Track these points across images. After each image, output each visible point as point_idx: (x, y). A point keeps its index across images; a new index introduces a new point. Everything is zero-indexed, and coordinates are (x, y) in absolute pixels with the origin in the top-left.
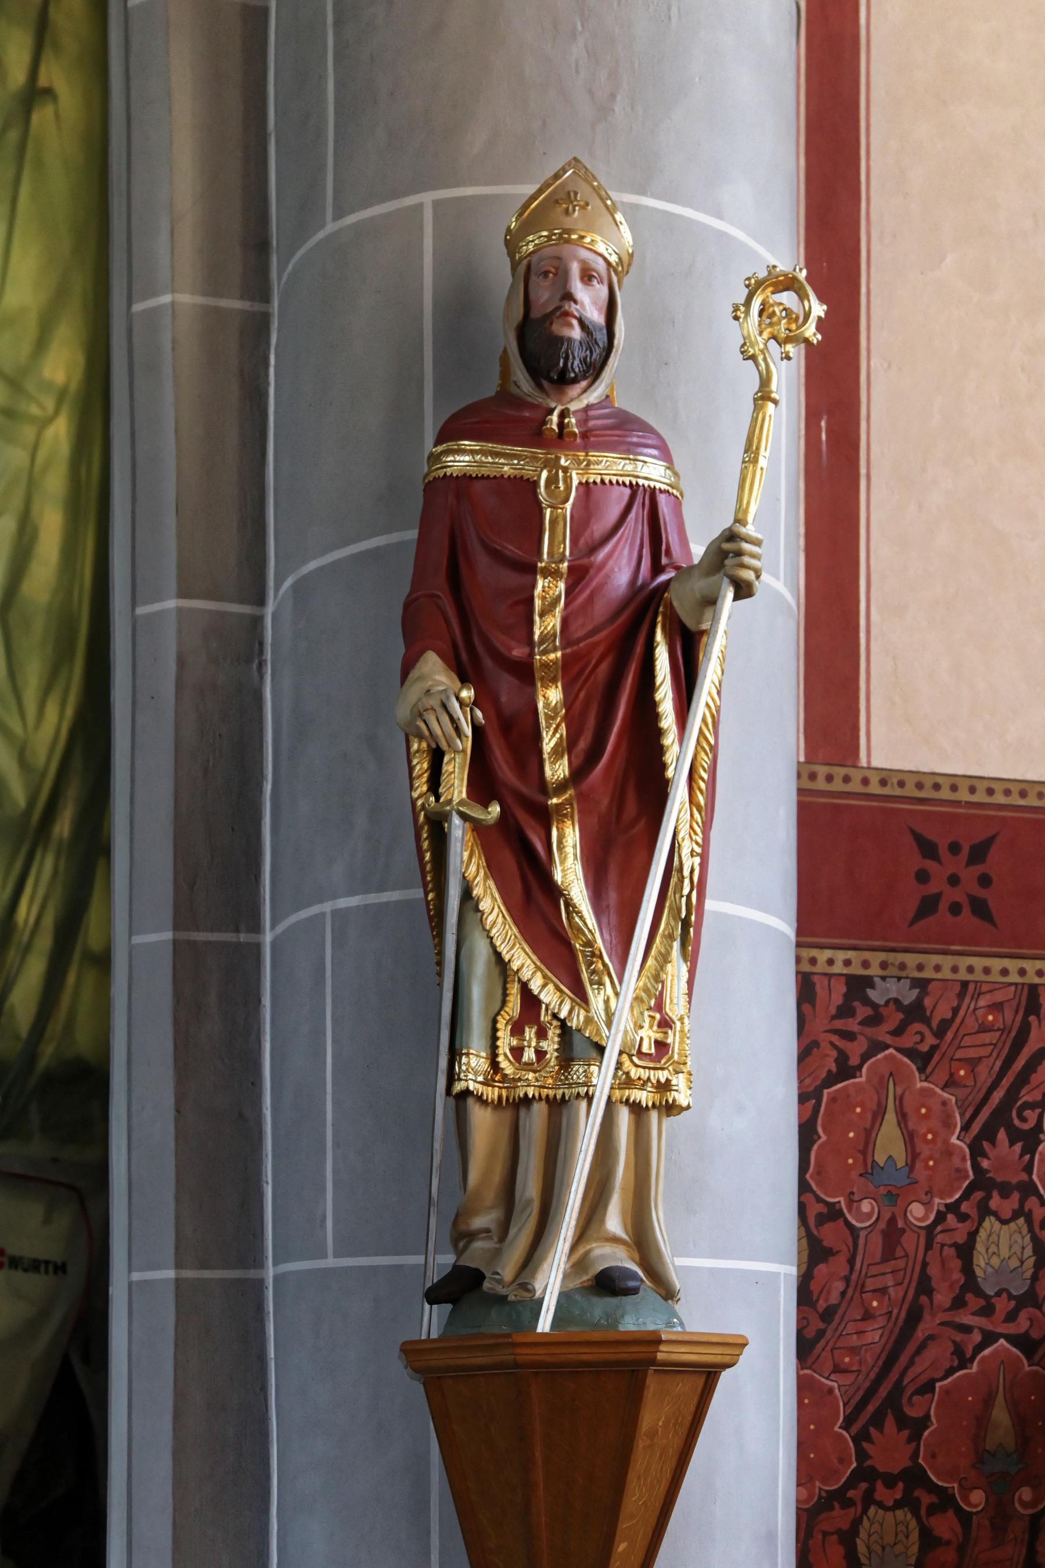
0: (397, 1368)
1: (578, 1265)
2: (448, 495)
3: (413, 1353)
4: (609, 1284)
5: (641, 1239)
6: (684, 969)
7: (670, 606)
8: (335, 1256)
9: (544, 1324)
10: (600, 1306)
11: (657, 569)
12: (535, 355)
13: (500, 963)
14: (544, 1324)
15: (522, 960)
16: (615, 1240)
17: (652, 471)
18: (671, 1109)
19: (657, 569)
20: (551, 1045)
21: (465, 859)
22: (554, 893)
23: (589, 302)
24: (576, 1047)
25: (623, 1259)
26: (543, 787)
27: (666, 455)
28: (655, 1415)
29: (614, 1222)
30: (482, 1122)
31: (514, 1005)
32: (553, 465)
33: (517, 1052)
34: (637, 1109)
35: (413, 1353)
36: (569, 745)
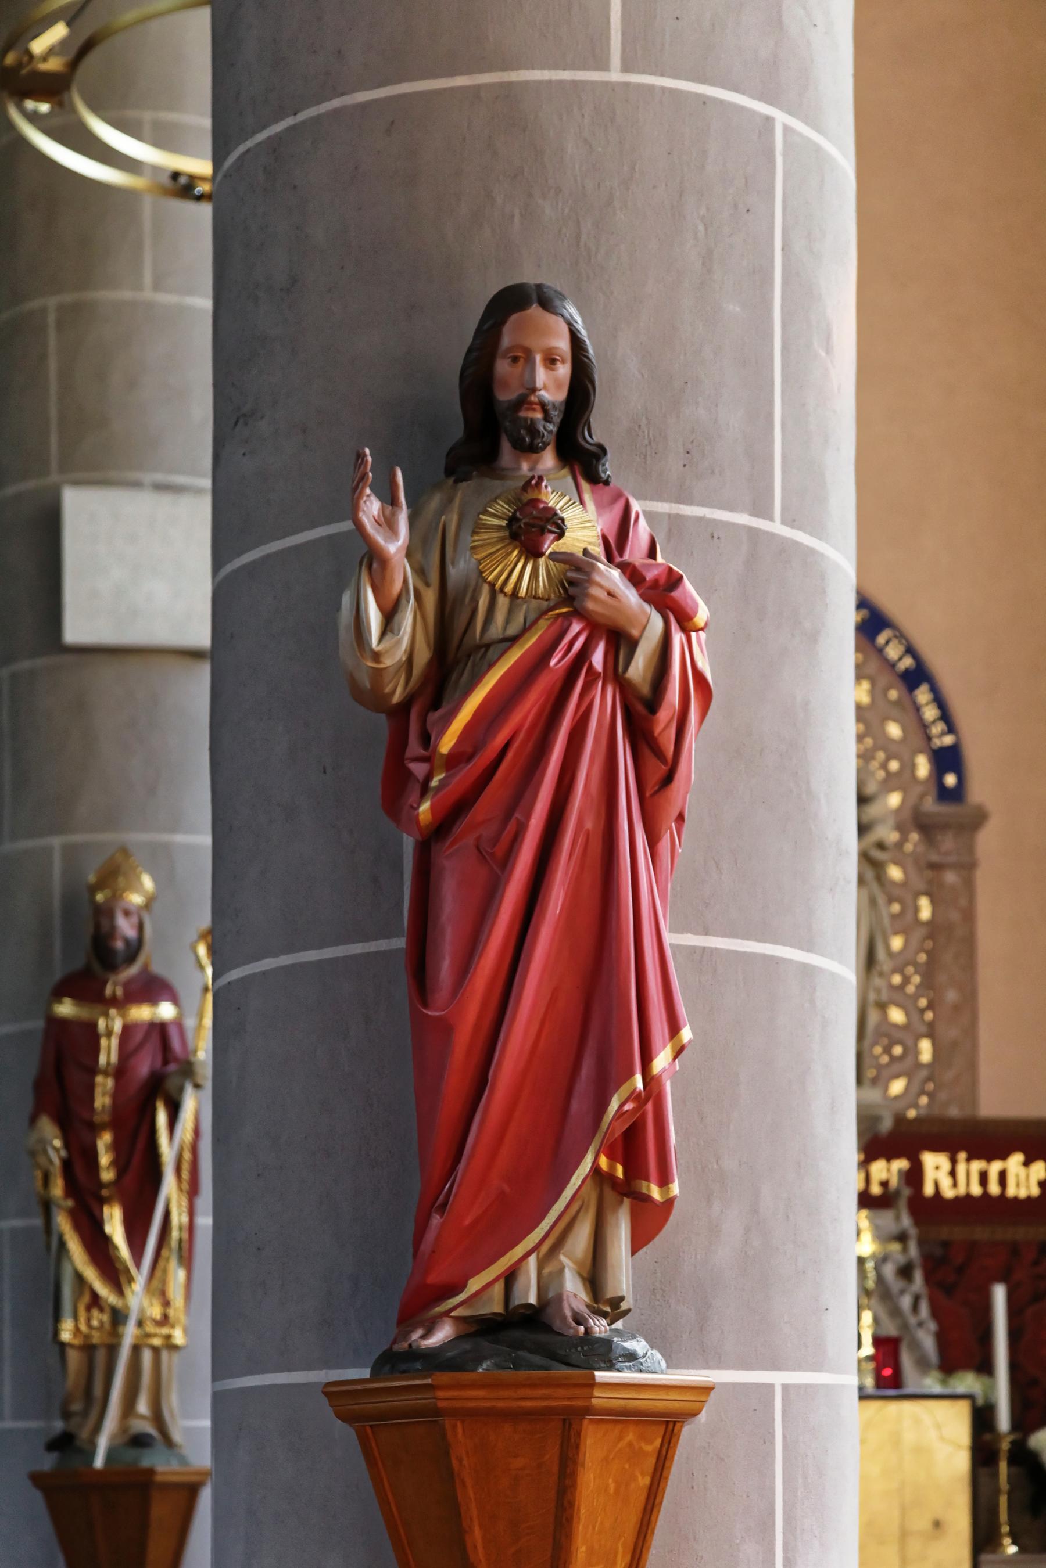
0: (28, 1483)
1: (123, 1429)
2: (57, 1026)
3: (37, 1479)
4: (140, 1441)
5: (158, 1417)
6: (181, 1274)
7: (591, 664)
8: (771, 1387)
9: (99, 1462)
10: (130, 1454)
11: (166, 1062)
12: (99, 959)
13: (79, 1278)
14: (99, 1462)
15: (91, 1274)
16: (143, 1417)
17: (166, 1011)
18: (174, 1348)
19: (166, 1062)
20: (105, 1318)
21: (63, 1223)
22: (107, 1240)
23: (126, 927)
24: (118, 1317)
25: (149, 1428)
26: (101, 1185)
27: (175, 1000)
28: (160, 1510)
29: (143, 1407)
30: (73, 1358)
31: (86, 1298)
32: (106, 1015)
33: (89, 1320)
34: (156, 1350)
35: (37, 1479)
36: (115, 1163)
